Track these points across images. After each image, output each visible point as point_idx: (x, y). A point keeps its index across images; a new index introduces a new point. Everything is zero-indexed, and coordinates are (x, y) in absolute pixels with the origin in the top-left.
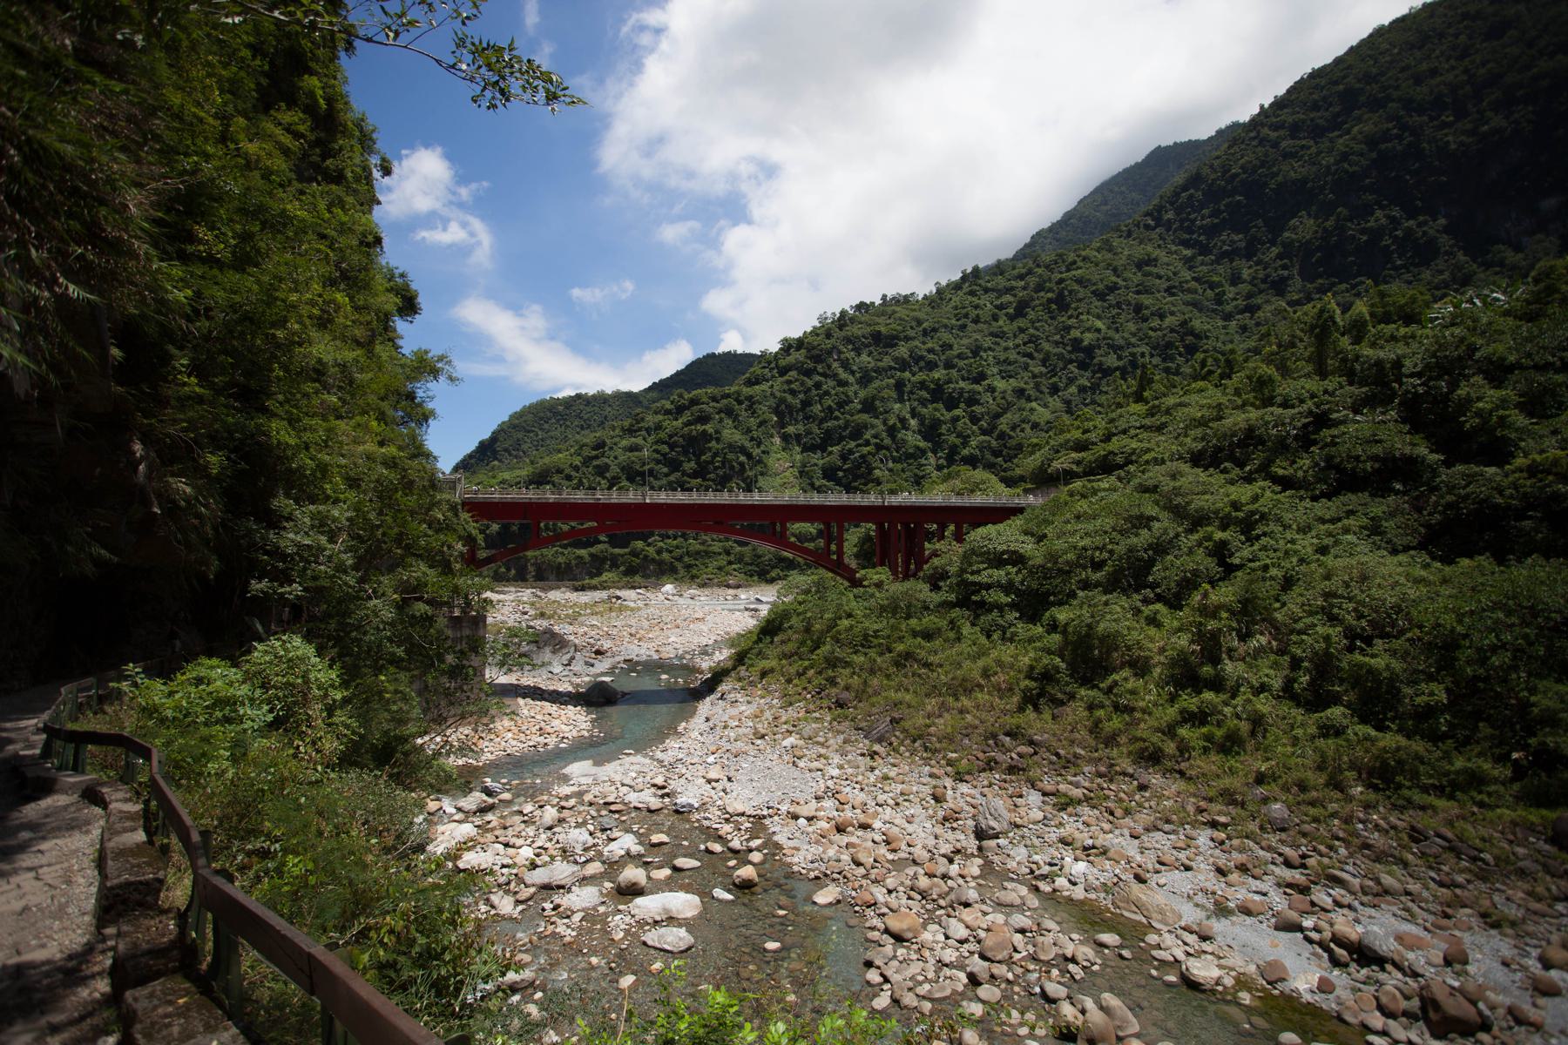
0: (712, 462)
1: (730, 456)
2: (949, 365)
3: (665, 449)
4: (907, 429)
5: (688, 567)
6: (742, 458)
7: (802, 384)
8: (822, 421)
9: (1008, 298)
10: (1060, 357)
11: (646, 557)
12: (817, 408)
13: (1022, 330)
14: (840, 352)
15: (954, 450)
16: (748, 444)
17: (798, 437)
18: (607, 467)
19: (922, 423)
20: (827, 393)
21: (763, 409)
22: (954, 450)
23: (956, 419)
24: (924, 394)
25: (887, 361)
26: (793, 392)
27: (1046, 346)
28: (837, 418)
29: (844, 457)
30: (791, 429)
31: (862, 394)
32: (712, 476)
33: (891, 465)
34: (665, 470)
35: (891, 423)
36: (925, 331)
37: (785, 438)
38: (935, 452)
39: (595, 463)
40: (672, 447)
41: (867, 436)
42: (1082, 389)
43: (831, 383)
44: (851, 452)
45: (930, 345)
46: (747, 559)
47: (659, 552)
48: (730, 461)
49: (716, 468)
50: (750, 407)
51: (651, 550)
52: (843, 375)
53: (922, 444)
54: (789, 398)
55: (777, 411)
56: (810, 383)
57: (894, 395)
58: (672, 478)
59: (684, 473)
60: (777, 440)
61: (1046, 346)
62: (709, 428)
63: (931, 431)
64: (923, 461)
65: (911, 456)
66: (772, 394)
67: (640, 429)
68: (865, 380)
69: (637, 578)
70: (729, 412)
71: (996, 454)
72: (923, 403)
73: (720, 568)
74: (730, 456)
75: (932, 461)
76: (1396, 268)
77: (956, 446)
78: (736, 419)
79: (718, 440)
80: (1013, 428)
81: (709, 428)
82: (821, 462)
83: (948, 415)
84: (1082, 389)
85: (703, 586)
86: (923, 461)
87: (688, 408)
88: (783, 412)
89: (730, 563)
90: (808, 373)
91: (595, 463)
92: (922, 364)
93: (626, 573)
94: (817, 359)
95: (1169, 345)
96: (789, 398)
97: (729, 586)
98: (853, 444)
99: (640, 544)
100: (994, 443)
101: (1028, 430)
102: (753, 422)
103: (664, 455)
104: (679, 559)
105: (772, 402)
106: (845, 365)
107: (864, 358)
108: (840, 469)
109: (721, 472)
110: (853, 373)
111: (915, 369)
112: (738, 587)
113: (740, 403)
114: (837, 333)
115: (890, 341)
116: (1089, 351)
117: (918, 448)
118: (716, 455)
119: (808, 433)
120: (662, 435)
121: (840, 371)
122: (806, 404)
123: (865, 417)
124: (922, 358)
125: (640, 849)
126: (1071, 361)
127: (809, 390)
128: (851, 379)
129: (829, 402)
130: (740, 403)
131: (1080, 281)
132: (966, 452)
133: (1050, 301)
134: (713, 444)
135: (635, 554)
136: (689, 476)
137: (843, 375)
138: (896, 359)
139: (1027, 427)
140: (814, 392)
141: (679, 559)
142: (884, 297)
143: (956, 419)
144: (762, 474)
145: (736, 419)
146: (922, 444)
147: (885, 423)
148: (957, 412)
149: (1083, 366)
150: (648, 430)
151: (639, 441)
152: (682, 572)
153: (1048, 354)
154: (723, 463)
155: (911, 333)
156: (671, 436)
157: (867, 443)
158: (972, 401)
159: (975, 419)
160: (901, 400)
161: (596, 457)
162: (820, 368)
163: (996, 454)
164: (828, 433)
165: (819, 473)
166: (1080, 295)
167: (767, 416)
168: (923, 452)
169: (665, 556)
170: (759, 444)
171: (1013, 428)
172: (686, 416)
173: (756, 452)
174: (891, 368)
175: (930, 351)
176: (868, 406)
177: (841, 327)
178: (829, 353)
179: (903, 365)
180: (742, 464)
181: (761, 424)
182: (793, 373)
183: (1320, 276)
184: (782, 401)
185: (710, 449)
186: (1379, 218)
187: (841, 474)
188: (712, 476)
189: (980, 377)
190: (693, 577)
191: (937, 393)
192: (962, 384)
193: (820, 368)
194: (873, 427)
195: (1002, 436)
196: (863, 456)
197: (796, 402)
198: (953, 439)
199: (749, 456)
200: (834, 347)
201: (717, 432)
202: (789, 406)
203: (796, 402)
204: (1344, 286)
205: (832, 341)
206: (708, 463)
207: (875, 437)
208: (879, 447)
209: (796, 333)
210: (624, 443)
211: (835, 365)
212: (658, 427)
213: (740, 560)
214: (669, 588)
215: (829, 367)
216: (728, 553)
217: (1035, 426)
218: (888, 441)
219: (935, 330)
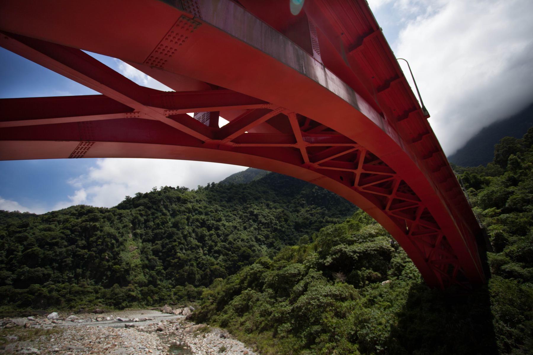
0: (96, 242)
1: (108, 239)
2: (207, 214)
3: (69, 232)
4: (191, 237)
5: (69, 301)
6: (114, 241)
7: (146, 212)
8: (153, 230)
9: (224, 195)
10: (246, 216)
11: (40, 294)
12: (152, 224)
13: (232, 206)
14: (164, 202)
15: (211, 247)
16: (117, 235)
17: (141, 235)
18: (26, 238)
19: (197, 235)
20: (157, 217)
21: (126, 220)
22: (211, 247)
23: (211, 235)
24: (198, 224)
25: (183, 208)
26: (141, 215)
27: (241, 213)
28: (161, 229)
29: (163, 246)
30: (138, 231)
31: (173, 220)
32: (94, 249)
33: (184, 251)
34: (66, 243)
35: (186, 233)
36: (197, 200)
37: (135, 235)
38: (203, 248)
39: (18, 235)
40: (73, 232)
41: (175, 238)
42: (255, 229)
43: (159, 214)
44: (167, 244)
45: (200, 205)
46: (108, 296)
47: (50, 291)
48: (107, 242)
49: (98, 245)
50: (119, 218)
51: (45, 290)
52: (165, 211)
53: (198, 244)
54: (140, 217)
55: (133, 222)
56: (150, 212)
57: (186, 222)
58: (70, 248)
59: (78, 246)
60: (131, 235)
61: (241, 213)
62: (98, 224)
63: (201, 238)
64: (198, 251)
65: (194, 248)
66: (131, 214)
67: (54, 221)
68: (174, 215)
69: (29, 309)
70: (109, 219)
71: (229, 250)
72: (197, 227)
73: (90, 301)
74: (108, 239)
75: (202, 251)
76: (331, 205)
77: (212, 246)
78: (112, 222)
79: (101, 231)
80: (235, 240)
81: (98, 224)
82: (151, 248)
83: (208, 233)
84: (255, 229)
85: (77, 313)
86: (198, 251)
87: (86, 214)
88: (135, 223)
89: (97, 298)
90: (149, 208)
91: (18, 235)
92: (197, 212)
93: (20, 306)
94: (154, 203)
95: (280, 217)
96: (140, 217)
97: (96, 312)
98: (168, 241)
99: (37, 286)
100: (227, 246)
101: (240, 242)
102: (120, 225)
103: (67, 235)
104: (64, 296)
105: (131, 218)
106: (166, 207)
107: (174, 205)
108: (161, 252)
109: (100, 247)
110: (169, 211)
111: (194, 214)
112: (102, 312)
113: (115, 215)
114: (163, 194)
115: (185, 201)
116: (256, 216)
117: (196, 245)
118: (99, 238)
119: (146, 234)
120: (68, 225)
121: (164, 209)
122: (146, 221)
123: (175, 230)
124: (197, 210)
125: (273, 330)
126: (250, 219)
127: (149, 215)
128: (168, 214)
129: (158, 221)
130: (115, 215)
131: (249, 193)
132: (216, 248)
133: (240, 198)
134: (98, 233)
135: (32, 292)
136: (80, 247)
137: (165, 211)
138: (186, 208)
139: (240, 240)
140: (151, 217)
141: (64, 296)
142: (178, 187)
143: (211, 235)
144: (123, 250)
145: (112, 222)
146: (198, 244)
147: (182, 233)
148: (211, 232)
149: (254, 221)
150: (59, 222)
151: (53, 226)
152: (64, 304)
153: (242, 215)
154: (102, 242)
155: (192, 200)
156: (73, 226)
157: (175, 241)
158: (217, 228)
159: (219, 236)
160: (188, 225)
161: (20, 232)
162: (154, 207)
163: (229, 250)
164: (156, 234)
165: (151, 253)
166: (250, 198)
167: (127, 224)
168: (198, 247)
169: (54, 294)
170: (122, 236)
171: (235, 240)
172: (84, 218)
173: (121, 239)
174: (184, 212)
175: (200, 207)
176: (176, 225)
177: (165, 192)
178: (160, 201)
179: (190, 211)
180: (113, 244)
181: (124, 227)
182: (141, 208)
183: (313, 204)
184: (136, 218)
185: (96, 235)
186: (304, 202)
187: (160, 254)
188: (94, 249)
189: (220, 220)
190: (71, 308)
191: (203, 224)
192: (212, 222)
193: (154, 207)
194: (177, 234)
195: (230, 243)
196: (173, 246)
197: (142, 219)
198: (210, 242)
199: (117, 241)
200: (162, 199)
201: (101, 227)
202: (139, 221)
203: (142, 219)
204: (319, 208)
205: (161, 196)
206: (93, 242)
207: (178, 238)
208: (180, 243)
209: (144, 192)
210: (41, 227)
211: (162, 207)
212: (67, 221)
213: (104, 296)
214: (54, 314)
215: (159, 207)
216: (97, 292)
217: (243, 240)
218: (183, 241)
219: (200, 200)
